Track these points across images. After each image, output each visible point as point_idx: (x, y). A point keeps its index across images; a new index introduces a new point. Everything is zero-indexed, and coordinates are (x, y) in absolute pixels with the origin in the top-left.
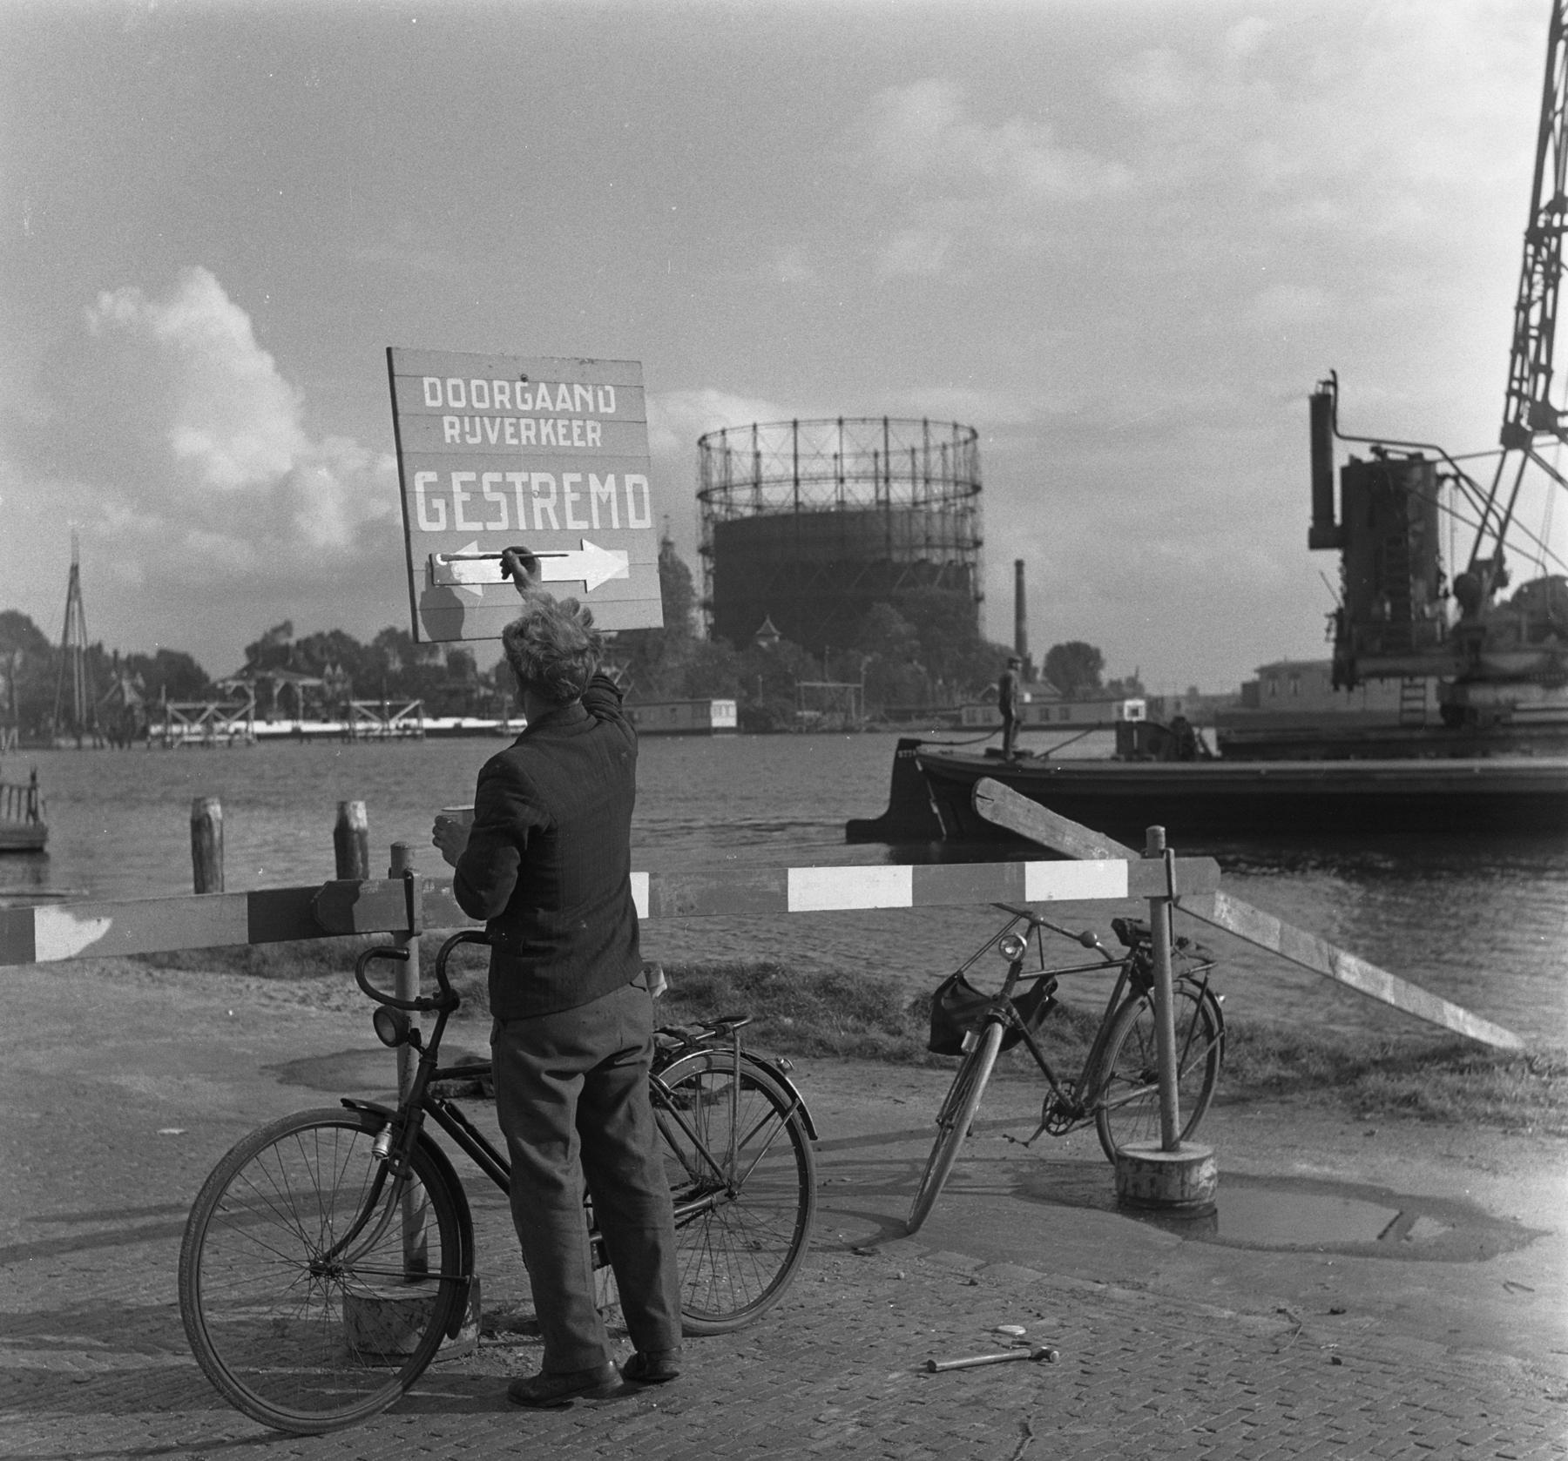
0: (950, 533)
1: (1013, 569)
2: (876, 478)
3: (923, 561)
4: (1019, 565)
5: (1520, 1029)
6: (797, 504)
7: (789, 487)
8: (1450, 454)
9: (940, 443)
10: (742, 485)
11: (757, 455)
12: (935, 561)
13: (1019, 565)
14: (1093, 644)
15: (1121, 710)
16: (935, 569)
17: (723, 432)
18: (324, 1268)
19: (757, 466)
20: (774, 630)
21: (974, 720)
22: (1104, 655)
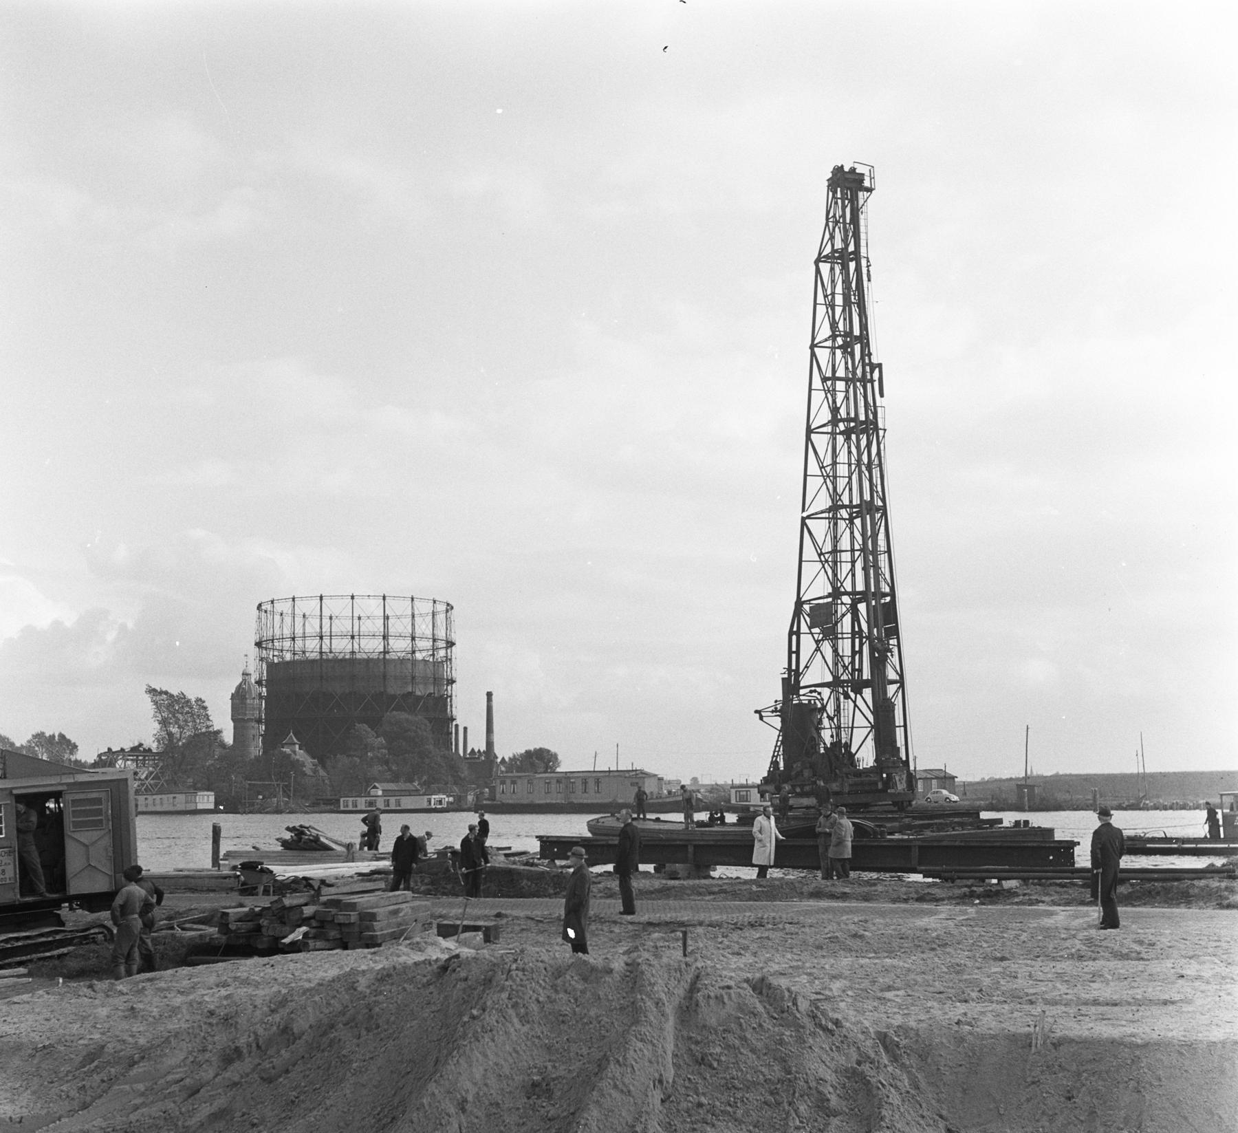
0: (429, 674)
1: (485, 697)
2: (353, 637)
3: (410, 694)
4: (489, 695)
5: (203, 1125)
6: (385, 652)
7: (409, 641)
8: (810, 635)
9: (280, 611)
10: (343, 636)
11: (386, 618)
12: (418, 693)
13: (489, 695)
14: (553, 750)
15: (429, 801)
16: (419, 698)
17: (272, 602)
18: (1190, 964)
19: (386, 626)
20: (295, 740)
21: (347, 806)
22: (560, 758)
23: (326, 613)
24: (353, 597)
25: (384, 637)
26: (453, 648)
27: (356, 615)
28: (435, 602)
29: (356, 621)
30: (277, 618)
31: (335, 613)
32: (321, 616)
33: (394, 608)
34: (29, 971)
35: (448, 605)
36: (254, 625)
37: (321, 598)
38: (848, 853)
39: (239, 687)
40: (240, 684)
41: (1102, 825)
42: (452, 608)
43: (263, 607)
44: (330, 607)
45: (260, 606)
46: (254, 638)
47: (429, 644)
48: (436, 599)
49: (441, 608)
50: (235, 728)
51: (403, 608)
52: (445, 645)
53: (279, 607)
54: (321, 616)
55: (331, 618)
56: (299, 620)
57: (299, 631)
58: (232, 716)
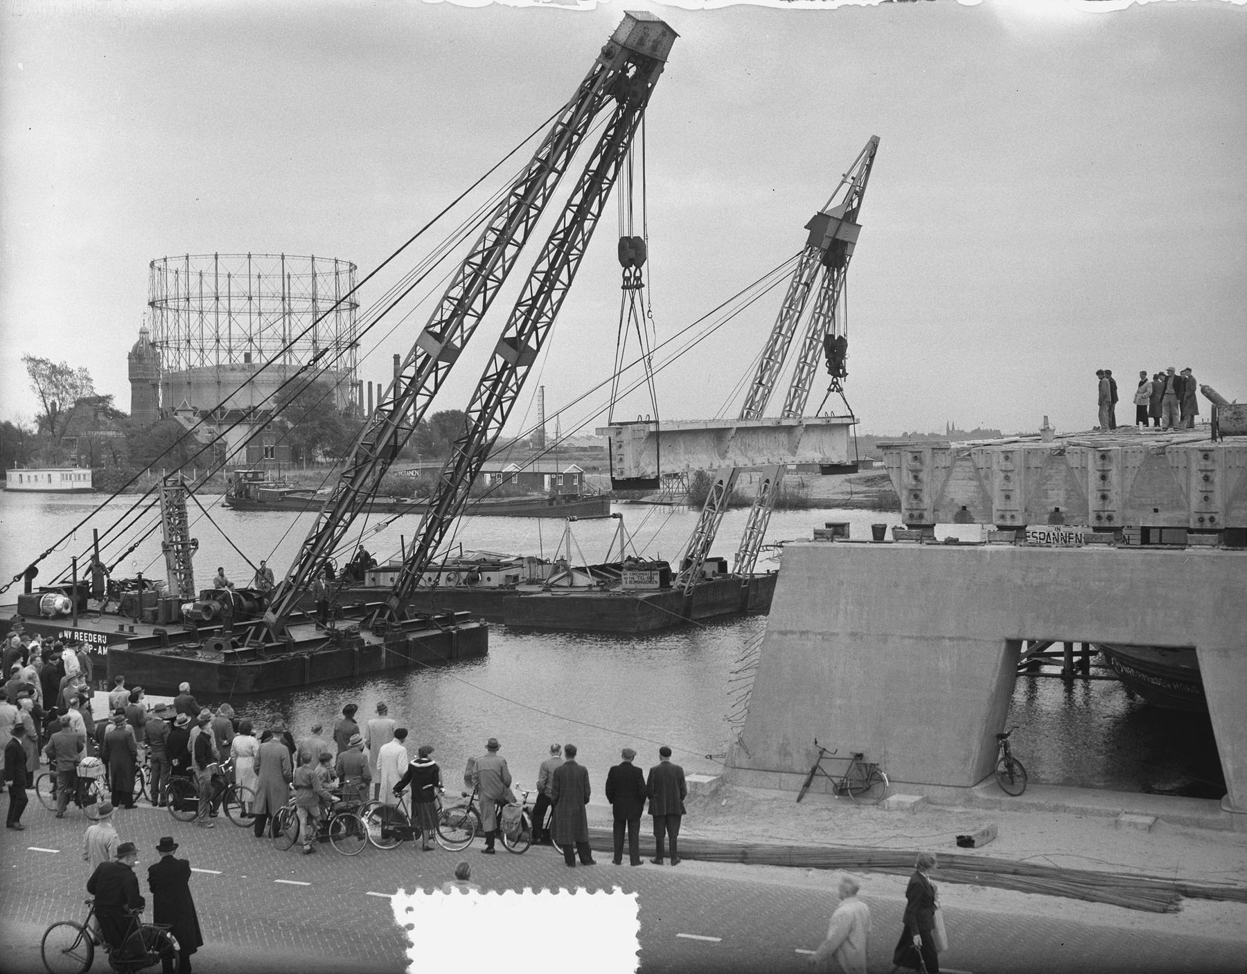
17: (165, 260)
23: (255, 272)
24: (249, 256)
25: (314, 300)
26: (357, 309)
27: (255, 272)
28: (336, 261)
29: (254, 280)
30: (171, 277)
31: (264, 272)
32: (217, 274)
33: (293, 266)
34: (120, 609)
35: (351, 264)
36: (147, 286)
37: (216, 256)
38: (383, 666)
39: (136, 347)
40: (138, 343)
41: (163, 858)
42: (356, 267)
43: (156, 265)
44: (259, 265)
45: (152, 264)
46: (146, 297)
47: (308, 304)
48: (338, 258)
49: (343, 267)
50: (133, 389)
51: (303, 267)
52: (349, 307)
53: (172, 265)
54: (217, 274)
55: (259, 277)
56: (223, 281)
57: (195, 291)
58: (130, 375)
